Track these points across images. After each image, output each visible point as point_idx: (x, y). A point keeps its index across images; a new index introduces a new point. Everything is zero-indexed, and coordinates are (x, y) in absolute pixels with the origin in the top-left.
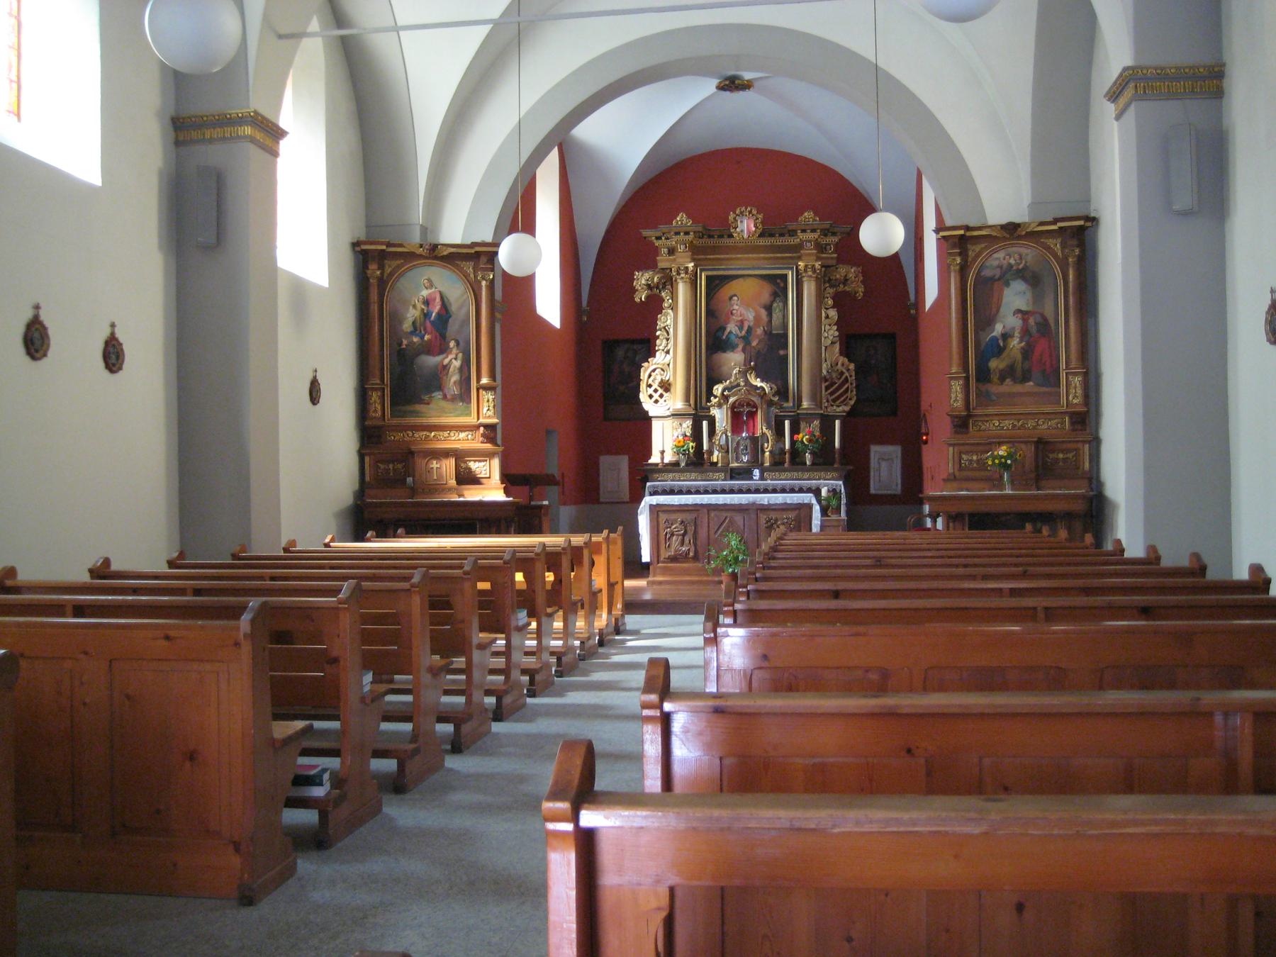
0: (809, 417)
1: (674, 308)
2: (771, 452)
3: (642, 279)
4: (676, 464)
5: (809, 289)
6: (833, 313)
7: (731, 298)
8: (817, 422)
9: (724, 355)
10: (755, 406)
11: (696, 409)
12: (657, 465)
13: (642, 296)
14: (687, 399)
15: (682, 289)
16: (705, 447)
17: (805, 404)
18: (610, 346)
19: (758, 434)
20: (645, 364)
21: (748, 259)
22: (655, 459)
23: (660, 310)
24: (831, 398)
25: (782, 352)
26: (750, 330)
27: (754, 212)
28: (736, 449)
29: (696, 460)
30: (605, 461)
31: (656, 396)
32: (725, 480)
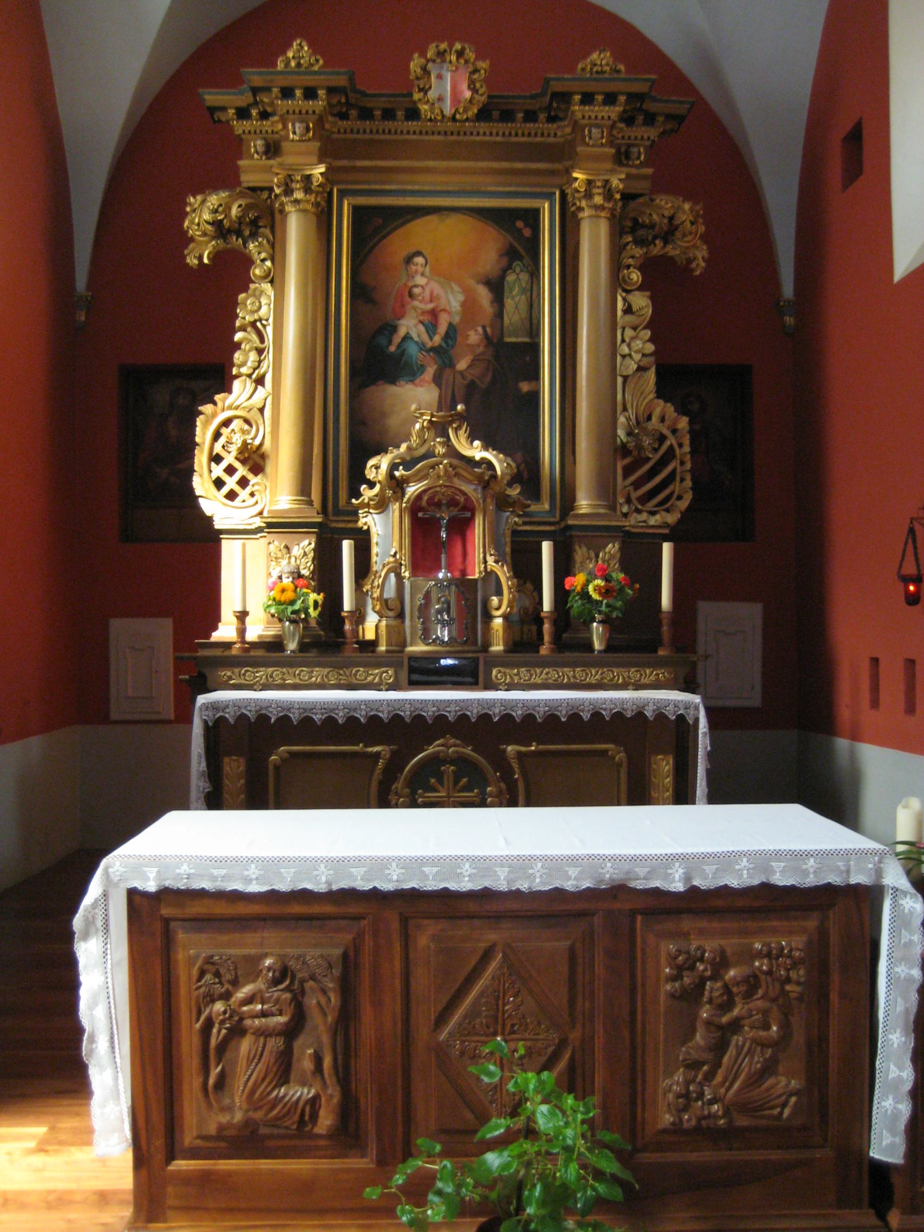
0: (596, 534)
1: (275, 279)
2: (505, 617)
3: (203, 211)
4: (275, 645)
5: (595, 238)
6: (641, 301)
7: (409, 260)
8: (612, 548)
9: (392, 389)
10: (469, 508)
11: (324, 510)
12: (228, 645)
13: (202, 253)
14: (304, 489)
15: (295, 229)
16: (347, 605)
17: (584, 504)
18: (137, 380)
19: (476, 573)
20: (207, 408)
21: (447, 171)
22: (226, 631)
23: (244, 283)
24: (635, 495)
25: (525, 387)
26: (452, 333)
27: (470, 55)
28: (424, 610)
29: (326, 638)
30: (121, 629)
31: (231, 483)
32: (394, 687)
